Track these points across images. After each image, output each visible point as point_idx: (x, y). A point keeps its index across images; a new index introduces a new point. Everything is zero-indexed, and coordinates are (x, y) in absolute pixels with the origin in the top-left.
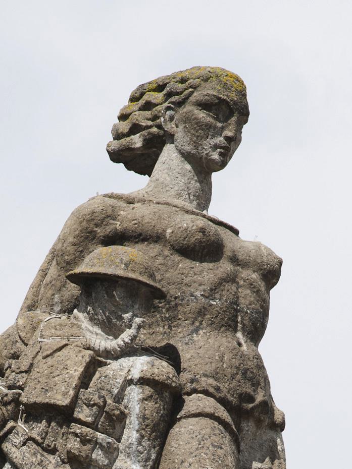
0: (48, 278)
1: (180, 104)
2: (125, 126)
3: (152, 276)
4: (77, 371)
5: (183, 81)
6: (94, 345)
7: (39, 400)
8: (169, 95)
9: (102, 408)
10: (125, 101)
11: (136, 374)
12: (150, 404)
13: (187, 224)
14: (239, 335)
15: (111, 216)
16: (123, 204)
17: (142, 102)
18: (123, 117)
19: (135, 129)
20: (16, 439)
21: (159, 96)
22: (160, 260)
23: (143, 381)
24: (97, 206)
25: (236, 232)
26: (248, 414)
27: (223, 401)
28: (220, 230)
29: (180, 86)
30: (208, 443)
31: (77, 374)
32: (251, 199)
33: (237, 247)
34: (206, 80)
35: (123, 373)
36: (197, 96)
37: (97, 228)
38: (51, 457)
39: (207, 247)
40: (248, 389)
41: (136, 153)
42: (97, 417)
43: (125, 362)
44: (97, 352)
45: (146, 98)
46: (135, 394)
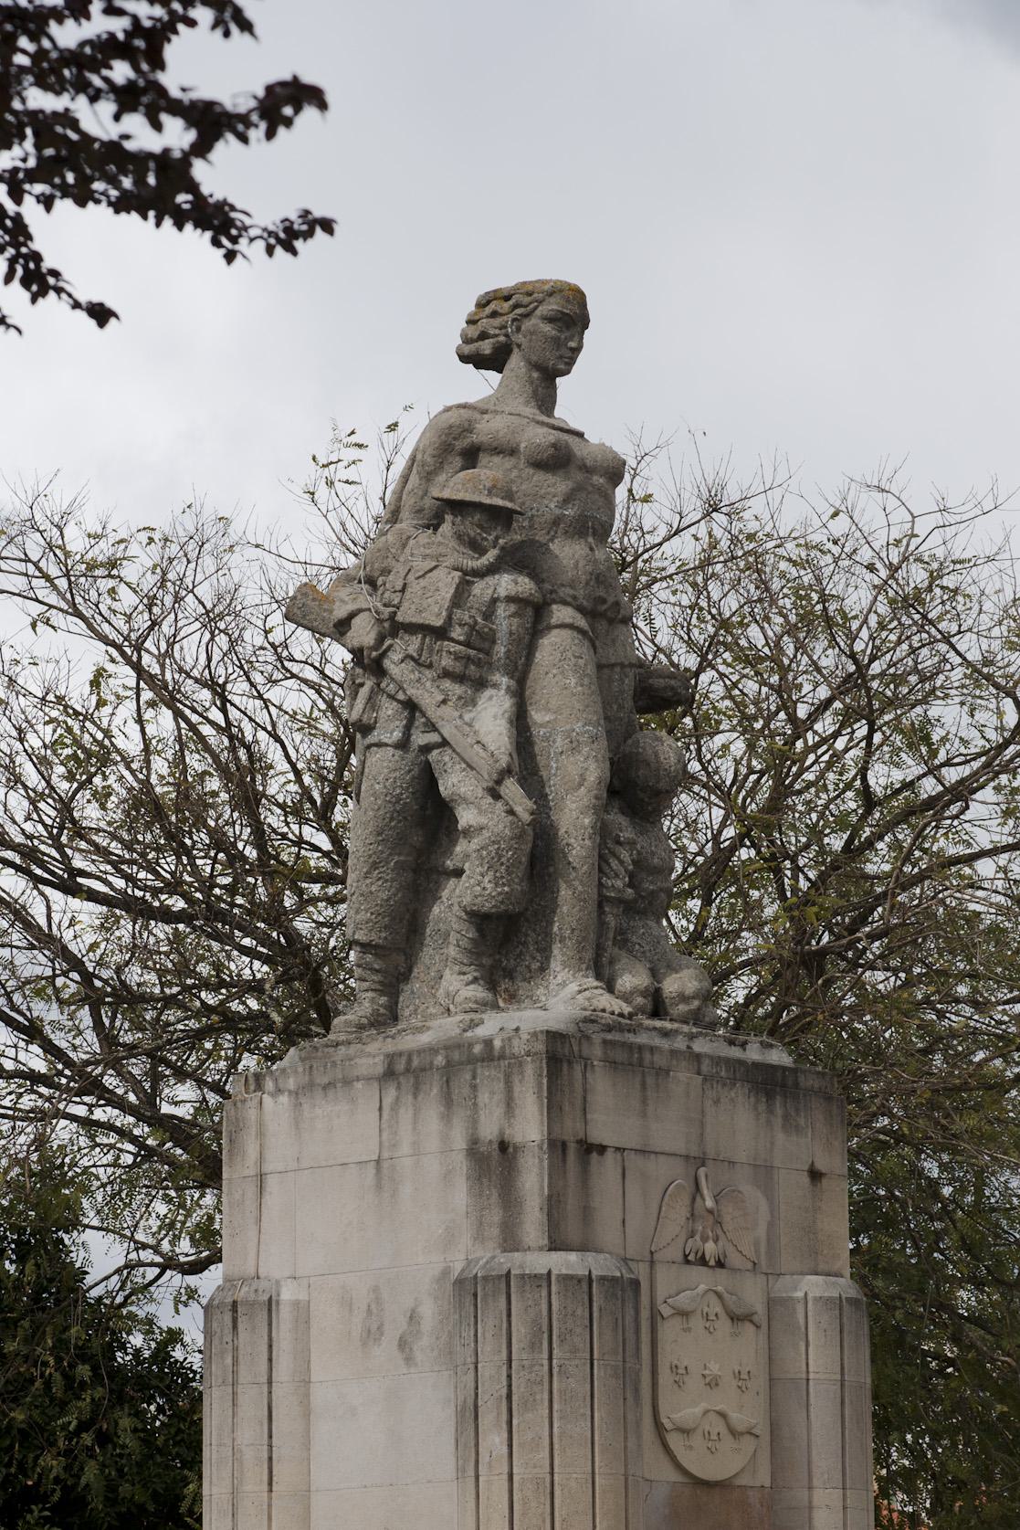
0: (409, 486)
1: (527, 316)
2: (474, 332)
3: (509, 496)
4: (448, 593)
5: (529, 294)
6: (644, 1085)
7: (414, 620)
8: (516, 306)
9: (472, 627)
10: (472, 308)
11: (502, 592)
12: (515, 620)
13: (536, 437)
14: (590, 539)
15: (467, 429)
16: (478, 416)
17: (488, 310)
18: (470, 322)
19: (483, 336)
20: (395, 656)
21: (506, 306)
22: (515, 473)
23: (510, 599)
24: (453, 418)
25: (580, 435)
26: (602, 615)
27: (580, 609)
28: (566, 437)
29: (526, 300)
30: (569, 654)
31: (449, 596)
32: (589, 403)
33: (585, 452)
34: (551, 294)
35: (490, 591)
36: (543, 310)
37: (457, 443)
38: (427, 672)
39: (562, 456)
40: (601, 592)
41: (484, 352)
42: (469, 635)
43: (490, 580)
44: (465, 573)
45: (492, 306)
46: (502, 611)
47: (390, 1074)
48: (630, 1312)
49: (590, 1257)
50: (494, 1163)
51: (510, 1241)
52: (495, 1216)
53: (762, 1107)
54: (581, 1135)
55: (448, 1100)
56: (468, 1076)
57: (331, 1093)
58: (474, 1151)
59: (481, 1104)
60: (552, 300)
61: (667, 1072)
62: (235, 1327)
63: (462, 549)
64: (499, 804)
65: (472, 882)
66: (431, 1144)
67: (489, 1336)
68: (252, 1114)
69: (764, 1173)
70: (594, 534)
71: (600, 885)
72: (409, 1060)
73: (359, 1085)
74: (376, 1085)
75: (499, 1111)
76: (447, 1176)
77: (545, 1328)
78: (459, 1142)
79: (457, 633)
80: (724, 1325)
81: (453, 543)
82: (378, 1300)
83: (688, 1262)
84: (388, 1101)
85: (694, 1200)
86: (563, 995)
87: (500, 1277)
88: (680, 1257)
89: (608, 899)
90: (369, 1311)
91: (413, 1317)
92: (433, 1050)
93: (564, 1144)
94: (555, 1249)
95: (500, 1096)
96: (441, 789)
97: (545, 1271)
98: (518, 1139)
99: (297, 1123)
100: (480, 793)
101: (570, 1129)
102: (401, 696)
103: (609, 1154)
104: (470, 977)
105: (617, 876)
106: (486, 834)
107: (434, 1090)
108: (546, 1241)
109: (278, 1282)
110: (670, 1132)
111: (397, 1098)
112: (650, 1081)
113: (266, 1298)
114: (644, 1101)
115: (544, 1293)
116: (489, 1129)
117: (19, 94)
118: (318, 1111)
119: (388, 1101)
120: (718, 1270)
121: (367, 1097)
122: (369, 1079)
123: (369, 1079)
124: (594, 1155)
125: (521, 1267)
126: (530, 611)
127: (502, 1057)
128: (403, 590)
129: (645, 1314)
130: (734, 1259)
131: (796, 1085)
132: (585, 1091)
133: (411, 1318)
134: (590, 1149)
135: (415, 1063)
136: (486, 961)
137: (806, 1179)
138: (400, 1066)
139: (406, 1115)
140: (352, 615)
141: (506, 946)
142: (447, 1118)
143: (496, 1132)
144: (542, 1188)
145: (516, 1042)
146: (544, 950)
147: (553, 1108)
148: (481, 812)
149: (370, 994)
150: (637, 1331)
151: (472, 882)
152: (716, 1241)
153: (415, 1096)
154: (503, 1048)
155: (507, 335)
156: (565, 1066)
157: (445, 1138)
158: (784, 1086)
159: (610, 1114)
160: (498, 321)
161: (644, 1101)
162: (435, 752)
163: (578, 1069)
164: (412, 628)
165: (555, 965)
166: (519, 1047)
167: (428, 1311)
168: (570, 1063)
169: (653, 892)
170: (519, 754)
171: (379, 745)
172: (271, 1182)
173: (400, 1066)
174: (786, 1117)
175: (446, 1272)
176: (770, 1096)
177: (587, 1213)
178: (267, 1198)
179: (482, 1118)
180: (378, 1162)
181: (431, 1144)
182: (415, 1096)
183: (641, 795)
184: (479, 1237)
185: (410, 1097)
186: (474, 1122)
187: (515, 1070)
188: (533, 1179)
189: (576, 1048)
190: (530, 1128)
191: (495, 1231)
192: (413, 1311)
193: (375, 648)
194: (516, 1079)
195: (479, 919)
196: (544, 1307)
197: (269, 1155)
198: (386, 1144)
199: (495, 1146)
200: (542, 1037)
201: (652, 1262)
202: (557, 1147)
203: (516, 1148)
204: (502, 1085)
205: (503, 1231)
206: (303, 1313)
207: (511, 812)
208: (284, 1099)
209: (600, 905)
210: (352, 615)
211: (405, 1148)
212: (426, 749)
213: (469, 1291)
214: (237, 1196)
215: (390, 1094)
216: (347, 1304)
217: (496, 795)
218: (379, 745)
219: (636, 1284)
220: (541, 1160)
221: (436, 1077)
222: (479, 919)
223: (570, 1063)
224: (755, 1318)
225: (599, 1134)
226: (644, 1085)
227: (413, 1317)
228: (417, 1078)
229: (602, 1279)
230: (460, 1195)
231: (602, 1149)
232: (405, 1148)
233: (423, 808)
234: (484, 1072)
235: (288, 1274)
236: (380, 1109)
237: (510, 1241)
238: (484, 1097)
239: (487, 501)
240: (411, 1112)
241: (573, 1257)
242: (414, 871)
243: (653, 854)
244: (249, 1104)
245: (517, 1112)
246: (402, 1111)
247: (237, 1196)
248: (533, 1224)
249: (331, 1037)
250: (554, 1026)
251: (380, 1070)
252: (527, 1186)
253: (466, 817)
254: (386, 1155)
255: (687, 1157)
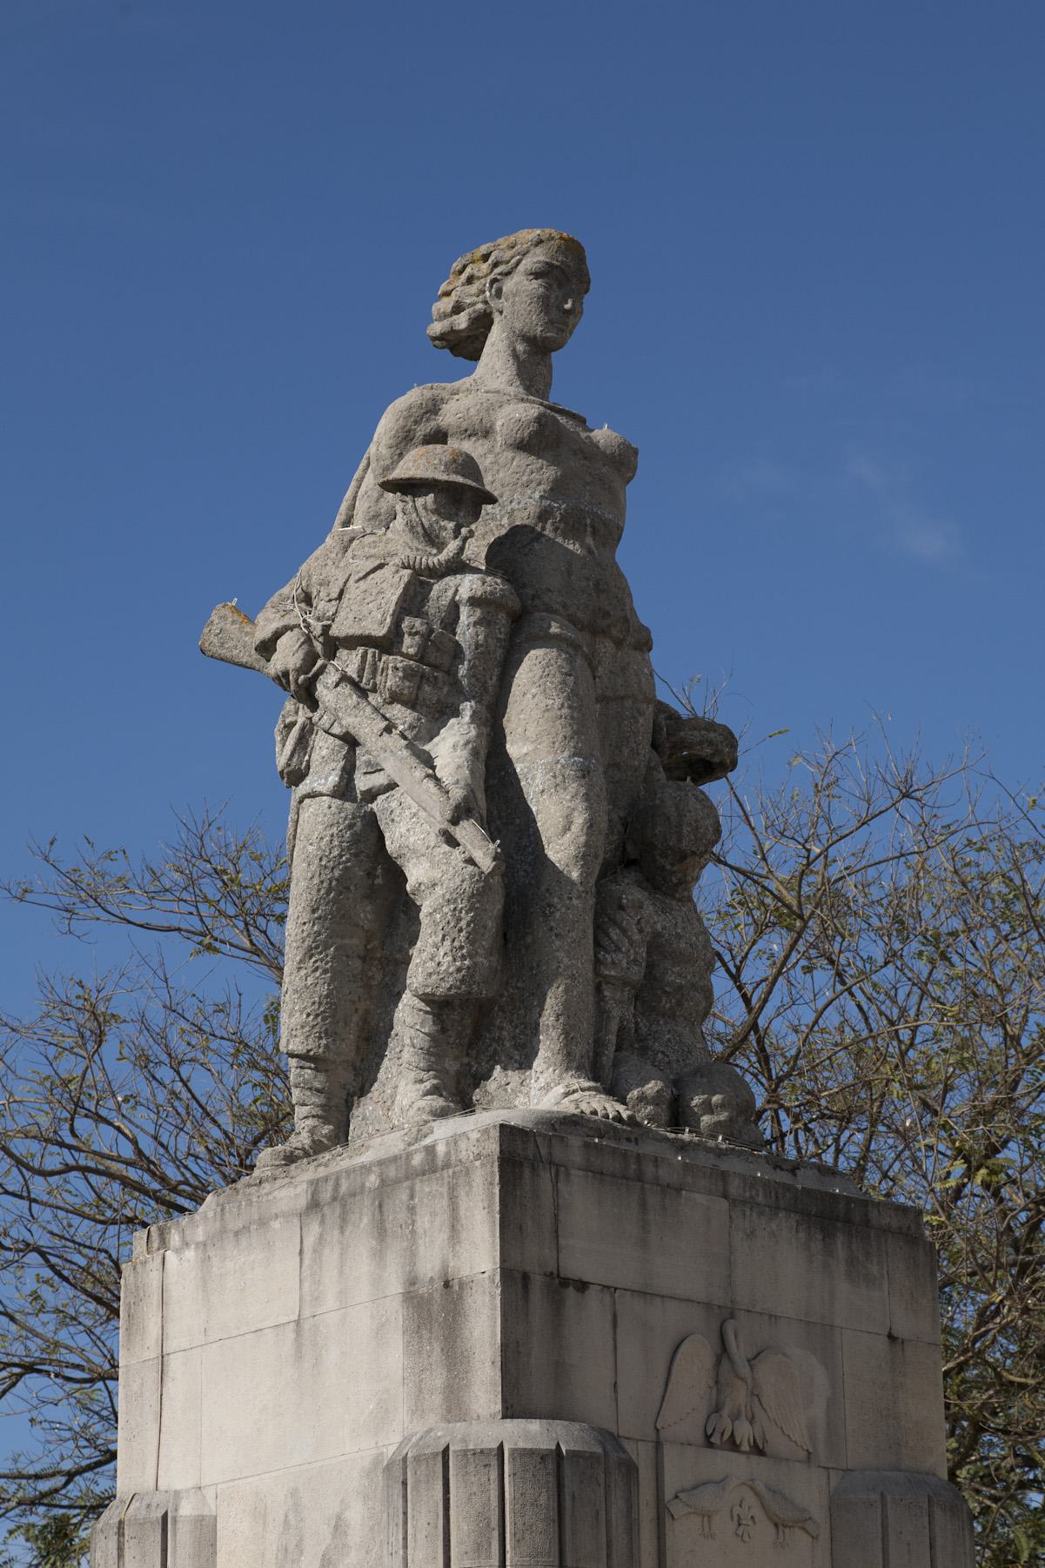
1: (508, 274)
6: (643, 1206)
7: (351, 632)
8: (496, 265)
12: (481, 629)
14: (589, 540)
20: (330, 677)
21: (485, 267)
23: (474, 602)
35: (450, 593)
43: (450, 581)
47: (314, 1205)
48: (618, 1505)
49: (559, 1427)
50: (434, 1309)
51: (455, 1406)
52: (438, 1379)
53: (817, 1246)
54: (552, 1267)
55: (381, 1231)
56: (405, 1197)
57: (244, 1240)
58: (414, 1299)
59: (420, 1231)
60: (538, 250)
61: (679, 1190)
62: (120, 1555)
63: (415, 544)
64: (456, 852)
65: (432, 960)
66: (360, 1294)
67: (421, 1536)
68: (153, 1277)
69: (821, 1335)
70: (594, 533)
71: (597, 962)
72: (337, 1186)
73: (276, 1225)
74: (296, 1221)
75: (443, 1236)
76: (380, 1330)
77: (495, 1522)
78: (395, 1285)
79: (409, 645)
80: (763, 1531)
81: (407, 537)
82: (297, 1507)
83: (710, 1445)
84: (310, 1241)
85: (718, 1363)
86: (543, 1089)
87: (435, 1455)
88: (698, 1436)
89: (608, 980)
90: (286, 1521)
91: (339, 1526)
92: (366, 1169)
93: (526, 1278)
94: (512, 1417)
95: (443, 1218)
96: (388, 843)
97: (495, 1445)
98: (465, 1272)
99: (204, 1281)
100: (433, 839)
101: (536, 1256)
102: (336, 730)
103: (593, 1292)
104: (428, 1085)
105: (618, 949)
106: (439, 891)
107: (364, 1219)
108: (499, 1407)
109: (177, 1493)
110: (682, 1266)
111: (321, 1236)
112: (653, 1200)
113: (160, 1514)
114: (645, 1226)
115: (494, 1475)
116: (429, 1266)
117: (615, 923)
118: (230, 1265)
119: (310, 1241)
120: (755, 1459)
121: (284, 1234)
122: (286, 1216)
123: (286, 1216)
124: (571, 1292)
125: (464, 1440)
126: (502, 618)
127: (447, 1166)
128: (340, 597)
129: (646, 1513)
130: (776, 1442)
131: (867, 1223)
132: (557, 1206)
133: (336, 1528)
134: (562, 1285)
135: (344, 1188)
136: (452, 1066)
137: (882, 1344)
138: (326, 1194)
139: (331, 1256)
140: (277, 635)
141: (475, 1040)
142: (379, 1255)
143: (438, 1267)
144: (494, 1332)
145: (463, 1145)
146: (524, 1046)
147: (511, 1227)
148: (433, 865)
149: (310, 1122)
150: (632, 1528)
151: (432, 960)
152: (752, 1421)
153: (342, 1230)
154: (448, 1153)
155: (486, 302)
156: (527, 1172)
157: (377, 1281)
158: (848, 1221)
159: (592, 1239)
160: (474, 288)
161: (645, 1226)
162: (381, 798)
163: (546, 1177)
164: (352, 642)
165: (538, 1063)
166: (466, 1151)
167: (356, 1515)
168: (534, 1169)
169: (680, 987)
170: (488, 789)
171: (312, 795)
172: (175, 1365)
173: (326, 1194)
174: (851, 1262)
175: (377, 1460)
176: (828, 1235)
177: (560, 1371)
178: (169, 1386)
179: (422, 1249)
180: (298, 1322)
181: (360, 1294)
182: (342, 1230)
183: (662, 861)
184: (417, 1410)
185: (336, 1232)
186: (412, 1255)
187: (461, 1181)
188: (483, 1324)
189: (544, 1151)
190: (480, 1257)
191: (437, 1399)
192: (339, 1518)
193: (299, 671)
194: (462, 1192)
195: (438, 1006)
196: (494, 1494)
197: (172, 1329)
198: (307, 1298)
199: (439, 1284)
200: (495, 1134)
201: (658, 1445)
202: (514, 1279)
203: (462, 1285)
204: (445, 1202)
205: (447, 1399)
206: (207, 1530)
207: (470, 861)
208: (190, 1254)
209: (598, 989)
210: (277, 635)
211: (330, 1302)
212: (371, 795)
213: (399, 1474)
214: (135, 1387)
215: (314, 1229)
216: (260, 1515)
217: (452, 842)
218: (312, 795)
219: (630, 1469)
220: (493, 1297)
221: (367, 1202)
222: (438, 1006)
223: (534, 1169)
224: (810, 1526)
225: (576, 1266)
226: (643, 1206)
227: (339, 1526)
228: (344, 1206)
229: (573, 1454)
230: (395, 1355)
231: (582, 1286)
232: (330, 1302)
233: (370, 874)
234: (424, 1187)
235: (190, 1484)
236: (301, 1252)
237: (455, 1406)
238: (423, 1221)
239: (444, 477)
240: (337, 1251)
241: (535, 1426)
242: (364, 959)
243: (679, 936)
244: (150, 1265)
245: (463, 1235)
246: (326, 1252)
247: (135, 1387)
248: (485, 1390)
249: (256, 1173)
250: (514, 1121)
251: (303, 1202)
252: (476, 1333)
253: (416, 873)
254: (307, 1313)
255: (708, 1306)
